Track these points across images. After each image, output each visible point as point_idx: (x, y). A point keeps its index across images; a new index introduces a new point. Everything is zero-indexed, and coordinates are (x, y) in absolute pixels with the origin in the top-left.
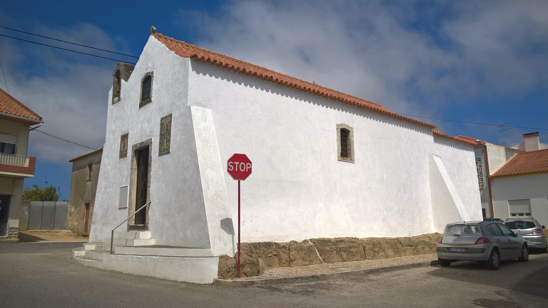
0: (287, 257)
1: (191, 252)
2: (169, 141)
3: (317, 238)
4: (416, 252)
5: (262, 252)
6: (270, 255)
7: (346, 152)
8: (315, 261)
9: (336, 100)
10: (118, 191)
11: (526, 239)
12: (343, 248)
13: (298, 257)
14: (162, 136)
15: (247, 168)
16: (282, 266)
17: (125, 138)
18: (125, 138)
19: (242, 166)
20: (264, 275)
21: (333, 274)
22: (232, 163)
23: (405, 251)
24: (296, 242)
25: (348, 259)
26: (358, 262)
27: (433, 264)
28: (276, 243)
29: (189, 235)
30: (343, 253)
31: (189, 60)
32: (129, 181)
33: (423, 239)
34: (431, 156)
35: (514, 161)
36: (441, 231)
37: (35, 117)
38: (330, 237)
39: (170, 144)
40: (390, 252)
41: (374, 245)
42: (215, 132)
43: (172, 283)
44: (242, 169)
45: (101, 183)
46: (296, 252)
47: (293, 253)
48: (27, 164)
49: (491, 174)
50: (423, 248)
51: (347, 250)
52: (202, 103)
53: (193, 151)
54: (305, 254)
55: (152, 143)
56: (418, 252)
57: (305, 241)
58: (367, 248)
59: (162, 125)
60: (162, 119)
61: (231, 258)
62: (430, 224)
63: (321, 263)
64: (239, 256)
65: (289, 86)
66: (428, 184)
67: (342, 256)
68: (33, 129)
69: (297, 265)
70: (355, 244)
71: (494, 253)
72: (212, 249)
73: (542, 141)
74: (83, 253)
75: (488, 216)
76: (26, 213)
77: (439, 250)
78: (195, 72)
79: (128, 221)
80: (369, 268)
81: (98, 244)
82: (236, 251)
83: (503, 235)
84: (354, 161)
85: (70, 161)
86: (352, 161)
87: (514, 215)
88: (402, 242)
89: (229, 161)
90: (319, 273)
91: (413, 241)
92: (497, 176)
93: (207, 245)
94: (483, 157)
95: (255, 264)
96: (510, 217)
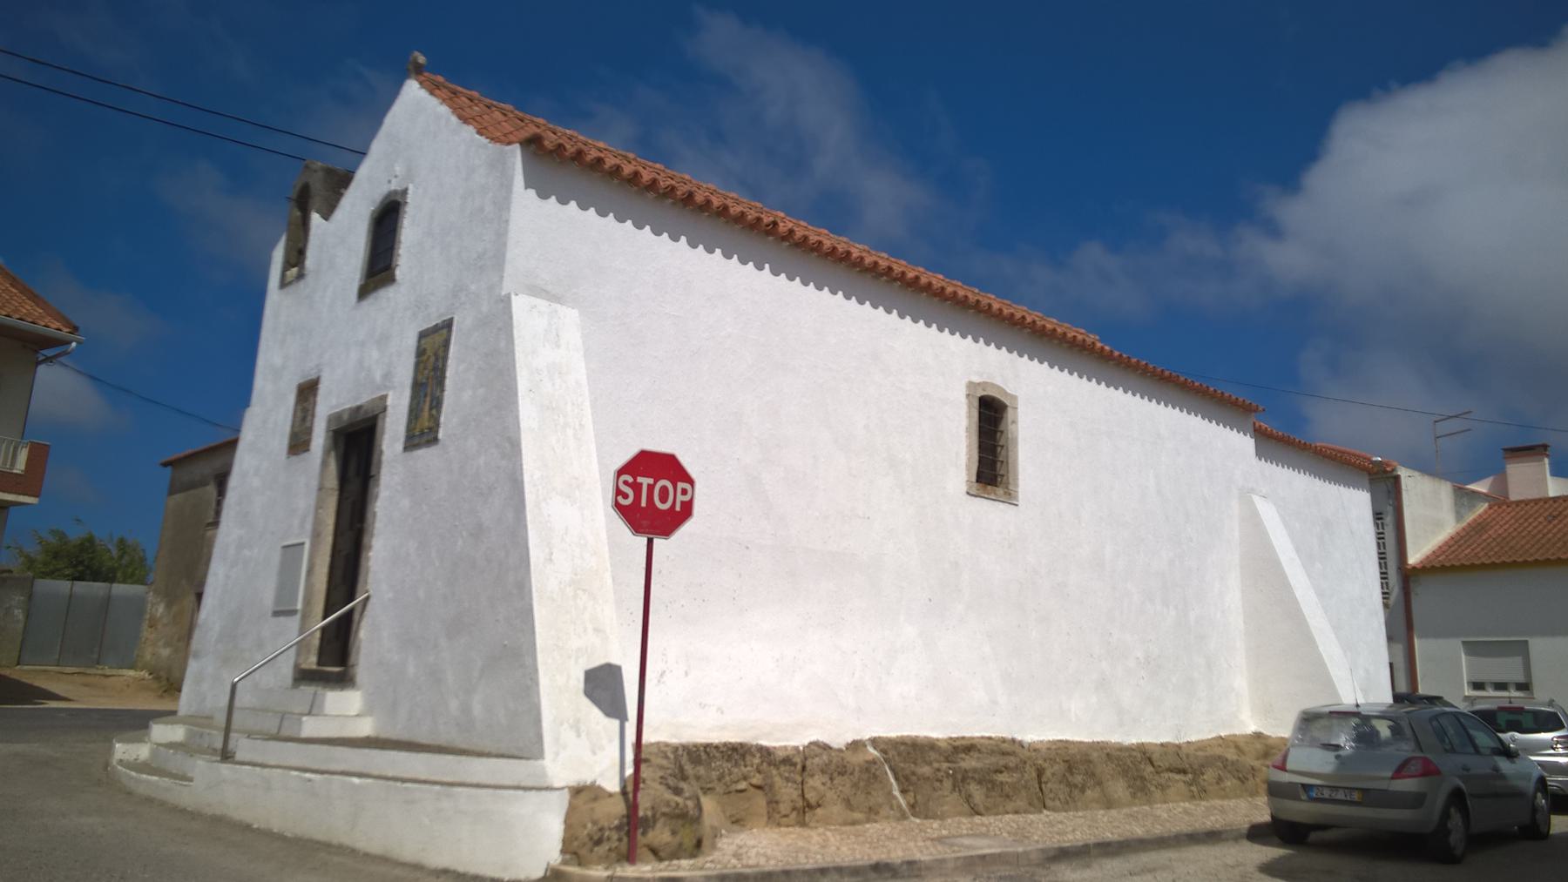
0: (795, 794)
1: (479, 769)
2: (437, 404)
3: (893, 734)
4: (1198, 792)
5: (714, 774)
6: (743, 785)
7: (992, 468)
8: (885, 811)
9: (970, 307)
10: (276, 557)
11: (1540, 763)
12: (975, 770)
13: (830, 795)
14: (418, 387)
15: (680, 498)
16: (779, 825)
17: (308, 391)
18: (308, 391)
19: (664, 490)
20: (716, 855)
21: (943, 861)
22: (630, 479)
23: (1163, 788)
24: (826, 747)
25: (987, 809)
26: (1020, 818)
27: (1256, 834)
28: (761, 749)
29: (477, 709)
30: (973, 788)
31: (515, 154)
32: (309, 527)
33: (1218, 751)
34: (1246, 495)
35: (1478, 528)
36: (1282, 728)
37: (57, 325)
38: (934, 735)
39: (439, 412)
40: (1119, 788)
41: (1070, 766)
42: (584, 381)
43: (398, 872)
44: (664, 499)
45: (228, 534)
46: (826, 779)
47: (816, 782)
48: (20, 466)
49: (1413, 559)
50: (1220, 780)
51: (986, 779)
52: (549, 288)
53: (509, 439)
54: (855, 785)
55: (385, 409)
56: (1202, 794)
57: (856, 746)
58: (1048, 773)
59: (420, 352)
60: (423, 335)
61: (611, 795)
62: (1241, 705)
63: (904, 817)
64: (636, 789)
65: (827, 254)
66: (1234, 580)
67: (969, 798)
68: (48, 360)
69: (826, 822)
70: (1012, 761)
71: (1452, 810)
72: (548, 762)
73: (1558, 472)
74: (143, 752)
75: (1403, 688)
76: (19, 614)
77: (1276, 791)
78: (532, 193)
79: (298, 654)
80: (1055, 842)
81: (197, 721)
82: (629, 771)
83: (1477, 750)
84: (1016, 498)
85: (165, 465)
86: (1010, 497)
87: (1478, 686)
88: (1155, 757)
89: (620, 472)
90: (896, 855)
91: (1188, 756)
92: (1430, 569)
93: (531, 749)
94: (1390, 509)
95: (687, 818)
96: (1468, 692)
